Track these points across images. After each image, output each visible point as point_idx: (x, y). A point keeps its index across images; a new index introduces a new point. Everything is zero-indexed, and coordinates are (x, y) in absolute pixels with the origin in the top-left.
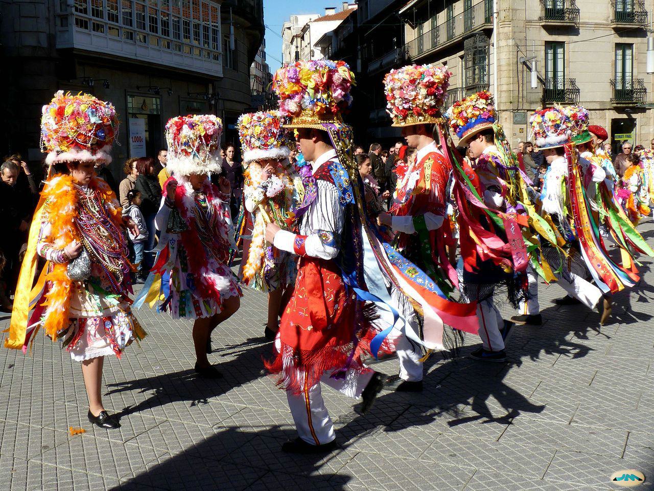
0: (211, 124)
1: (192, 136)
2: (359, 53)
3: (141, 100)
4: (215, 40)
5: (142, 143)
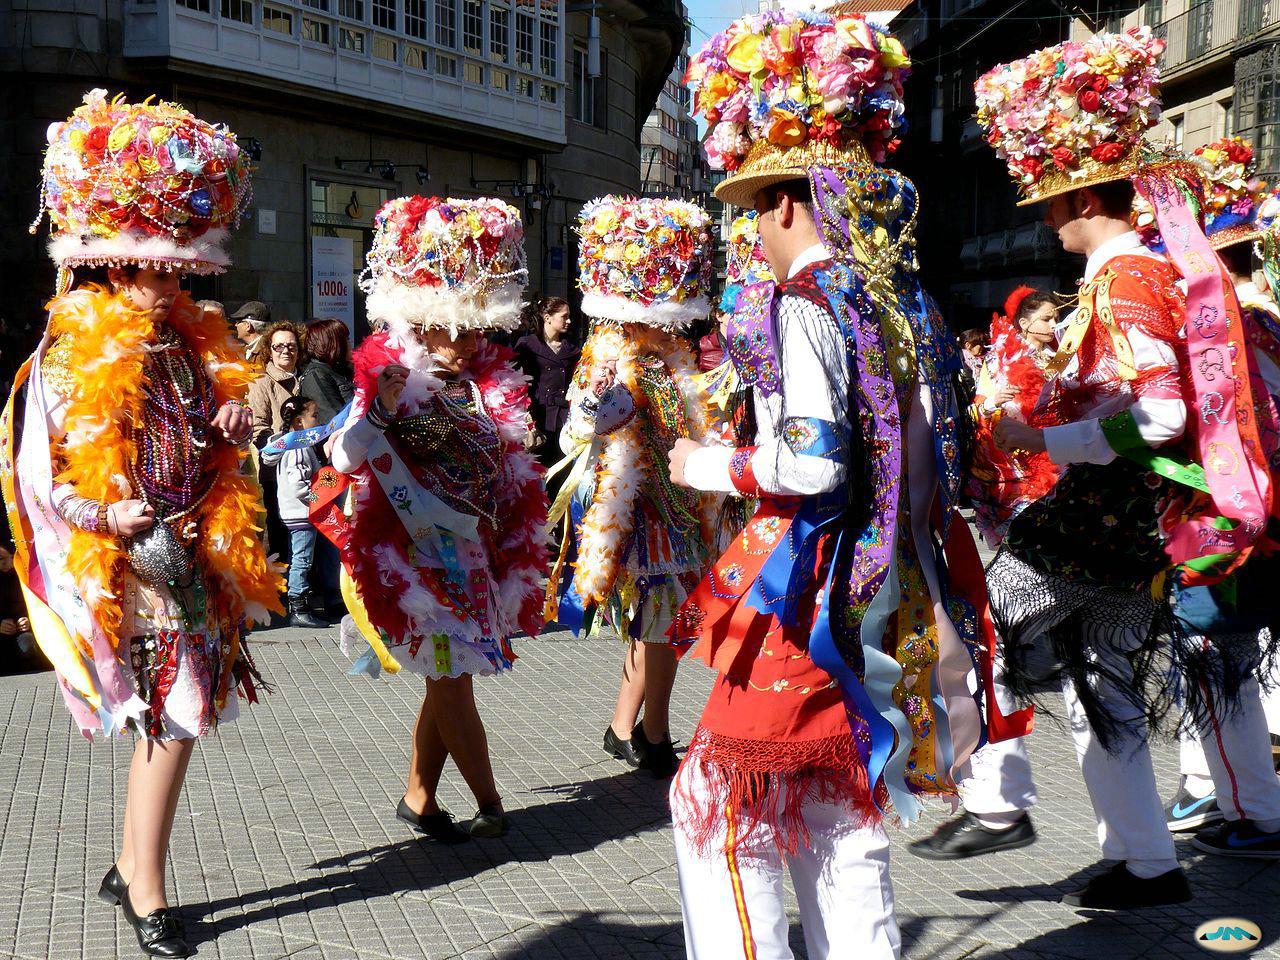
0: (498, 214)
1: (448, 238)
2: (940, 93)
3: (345, 193)
4: (548, 50)
5: (343, 299)
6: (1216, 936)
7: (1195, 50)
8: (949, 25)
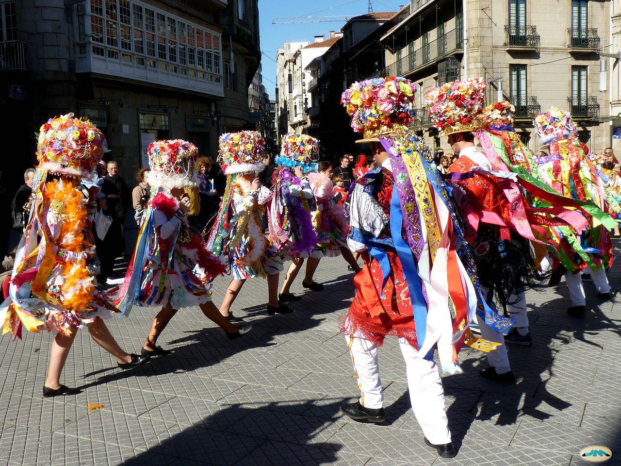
4: (217, 64)
6: (590, 454)
7: (425, 61)
8: (346, 52)
